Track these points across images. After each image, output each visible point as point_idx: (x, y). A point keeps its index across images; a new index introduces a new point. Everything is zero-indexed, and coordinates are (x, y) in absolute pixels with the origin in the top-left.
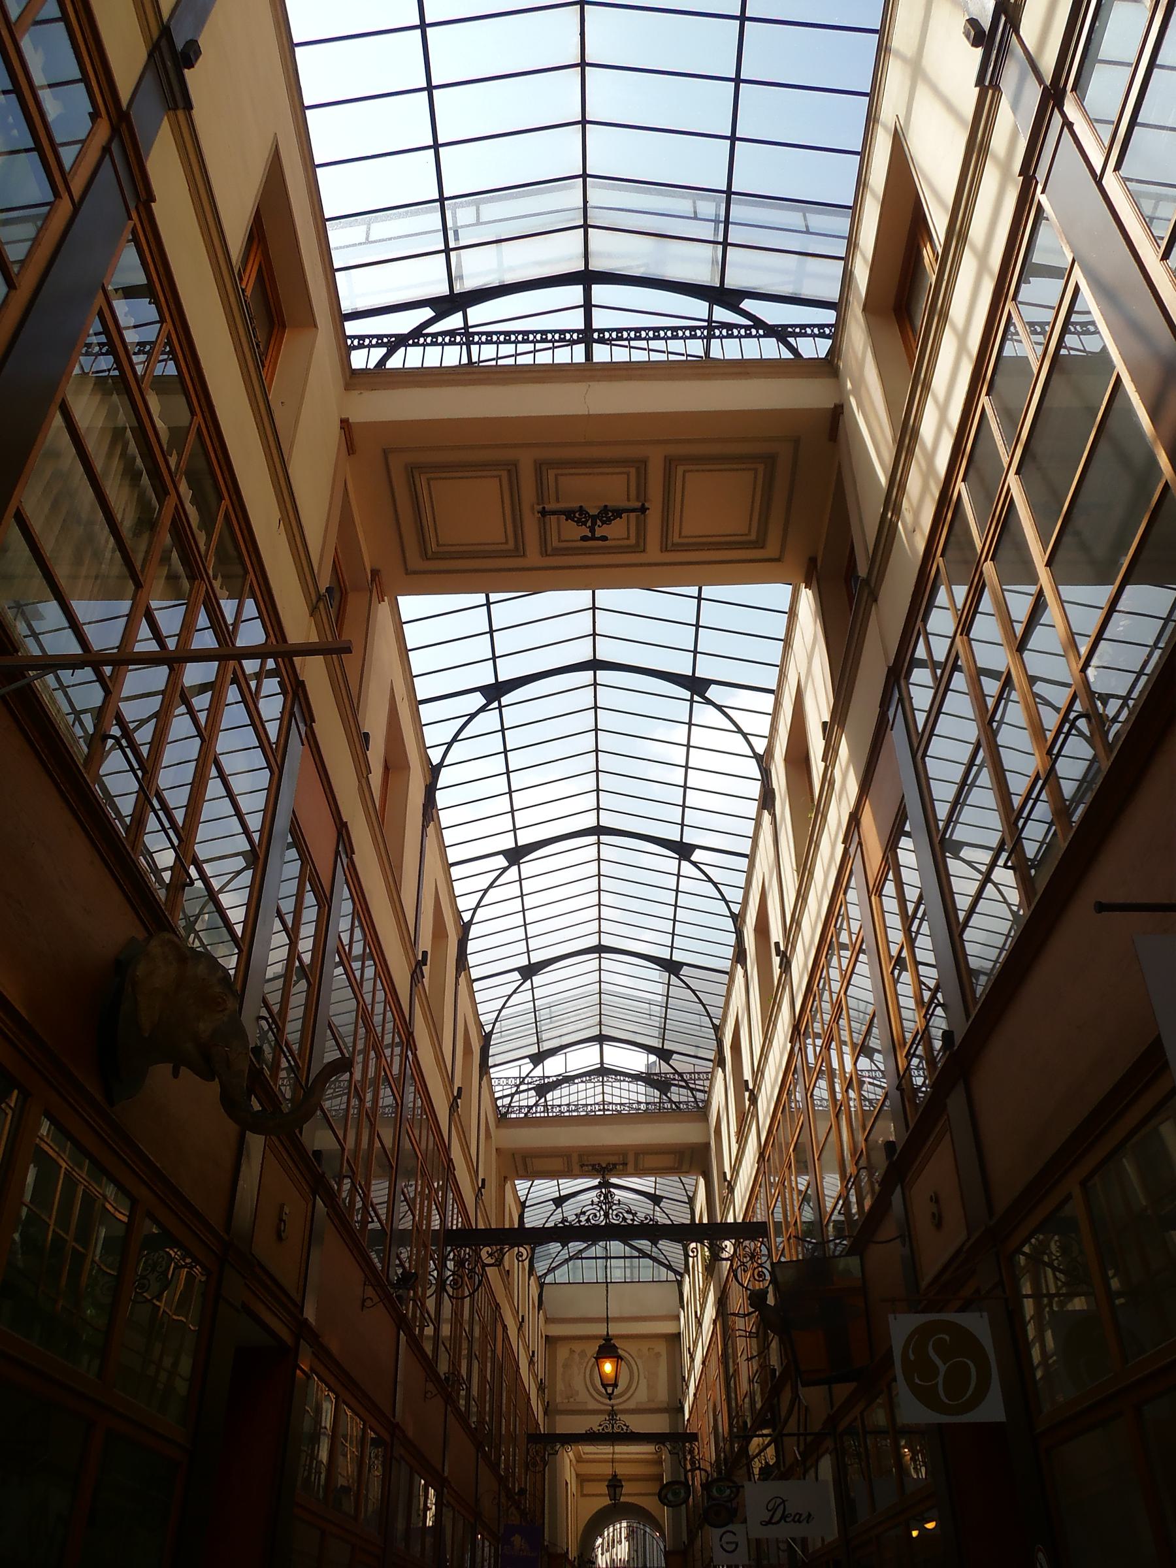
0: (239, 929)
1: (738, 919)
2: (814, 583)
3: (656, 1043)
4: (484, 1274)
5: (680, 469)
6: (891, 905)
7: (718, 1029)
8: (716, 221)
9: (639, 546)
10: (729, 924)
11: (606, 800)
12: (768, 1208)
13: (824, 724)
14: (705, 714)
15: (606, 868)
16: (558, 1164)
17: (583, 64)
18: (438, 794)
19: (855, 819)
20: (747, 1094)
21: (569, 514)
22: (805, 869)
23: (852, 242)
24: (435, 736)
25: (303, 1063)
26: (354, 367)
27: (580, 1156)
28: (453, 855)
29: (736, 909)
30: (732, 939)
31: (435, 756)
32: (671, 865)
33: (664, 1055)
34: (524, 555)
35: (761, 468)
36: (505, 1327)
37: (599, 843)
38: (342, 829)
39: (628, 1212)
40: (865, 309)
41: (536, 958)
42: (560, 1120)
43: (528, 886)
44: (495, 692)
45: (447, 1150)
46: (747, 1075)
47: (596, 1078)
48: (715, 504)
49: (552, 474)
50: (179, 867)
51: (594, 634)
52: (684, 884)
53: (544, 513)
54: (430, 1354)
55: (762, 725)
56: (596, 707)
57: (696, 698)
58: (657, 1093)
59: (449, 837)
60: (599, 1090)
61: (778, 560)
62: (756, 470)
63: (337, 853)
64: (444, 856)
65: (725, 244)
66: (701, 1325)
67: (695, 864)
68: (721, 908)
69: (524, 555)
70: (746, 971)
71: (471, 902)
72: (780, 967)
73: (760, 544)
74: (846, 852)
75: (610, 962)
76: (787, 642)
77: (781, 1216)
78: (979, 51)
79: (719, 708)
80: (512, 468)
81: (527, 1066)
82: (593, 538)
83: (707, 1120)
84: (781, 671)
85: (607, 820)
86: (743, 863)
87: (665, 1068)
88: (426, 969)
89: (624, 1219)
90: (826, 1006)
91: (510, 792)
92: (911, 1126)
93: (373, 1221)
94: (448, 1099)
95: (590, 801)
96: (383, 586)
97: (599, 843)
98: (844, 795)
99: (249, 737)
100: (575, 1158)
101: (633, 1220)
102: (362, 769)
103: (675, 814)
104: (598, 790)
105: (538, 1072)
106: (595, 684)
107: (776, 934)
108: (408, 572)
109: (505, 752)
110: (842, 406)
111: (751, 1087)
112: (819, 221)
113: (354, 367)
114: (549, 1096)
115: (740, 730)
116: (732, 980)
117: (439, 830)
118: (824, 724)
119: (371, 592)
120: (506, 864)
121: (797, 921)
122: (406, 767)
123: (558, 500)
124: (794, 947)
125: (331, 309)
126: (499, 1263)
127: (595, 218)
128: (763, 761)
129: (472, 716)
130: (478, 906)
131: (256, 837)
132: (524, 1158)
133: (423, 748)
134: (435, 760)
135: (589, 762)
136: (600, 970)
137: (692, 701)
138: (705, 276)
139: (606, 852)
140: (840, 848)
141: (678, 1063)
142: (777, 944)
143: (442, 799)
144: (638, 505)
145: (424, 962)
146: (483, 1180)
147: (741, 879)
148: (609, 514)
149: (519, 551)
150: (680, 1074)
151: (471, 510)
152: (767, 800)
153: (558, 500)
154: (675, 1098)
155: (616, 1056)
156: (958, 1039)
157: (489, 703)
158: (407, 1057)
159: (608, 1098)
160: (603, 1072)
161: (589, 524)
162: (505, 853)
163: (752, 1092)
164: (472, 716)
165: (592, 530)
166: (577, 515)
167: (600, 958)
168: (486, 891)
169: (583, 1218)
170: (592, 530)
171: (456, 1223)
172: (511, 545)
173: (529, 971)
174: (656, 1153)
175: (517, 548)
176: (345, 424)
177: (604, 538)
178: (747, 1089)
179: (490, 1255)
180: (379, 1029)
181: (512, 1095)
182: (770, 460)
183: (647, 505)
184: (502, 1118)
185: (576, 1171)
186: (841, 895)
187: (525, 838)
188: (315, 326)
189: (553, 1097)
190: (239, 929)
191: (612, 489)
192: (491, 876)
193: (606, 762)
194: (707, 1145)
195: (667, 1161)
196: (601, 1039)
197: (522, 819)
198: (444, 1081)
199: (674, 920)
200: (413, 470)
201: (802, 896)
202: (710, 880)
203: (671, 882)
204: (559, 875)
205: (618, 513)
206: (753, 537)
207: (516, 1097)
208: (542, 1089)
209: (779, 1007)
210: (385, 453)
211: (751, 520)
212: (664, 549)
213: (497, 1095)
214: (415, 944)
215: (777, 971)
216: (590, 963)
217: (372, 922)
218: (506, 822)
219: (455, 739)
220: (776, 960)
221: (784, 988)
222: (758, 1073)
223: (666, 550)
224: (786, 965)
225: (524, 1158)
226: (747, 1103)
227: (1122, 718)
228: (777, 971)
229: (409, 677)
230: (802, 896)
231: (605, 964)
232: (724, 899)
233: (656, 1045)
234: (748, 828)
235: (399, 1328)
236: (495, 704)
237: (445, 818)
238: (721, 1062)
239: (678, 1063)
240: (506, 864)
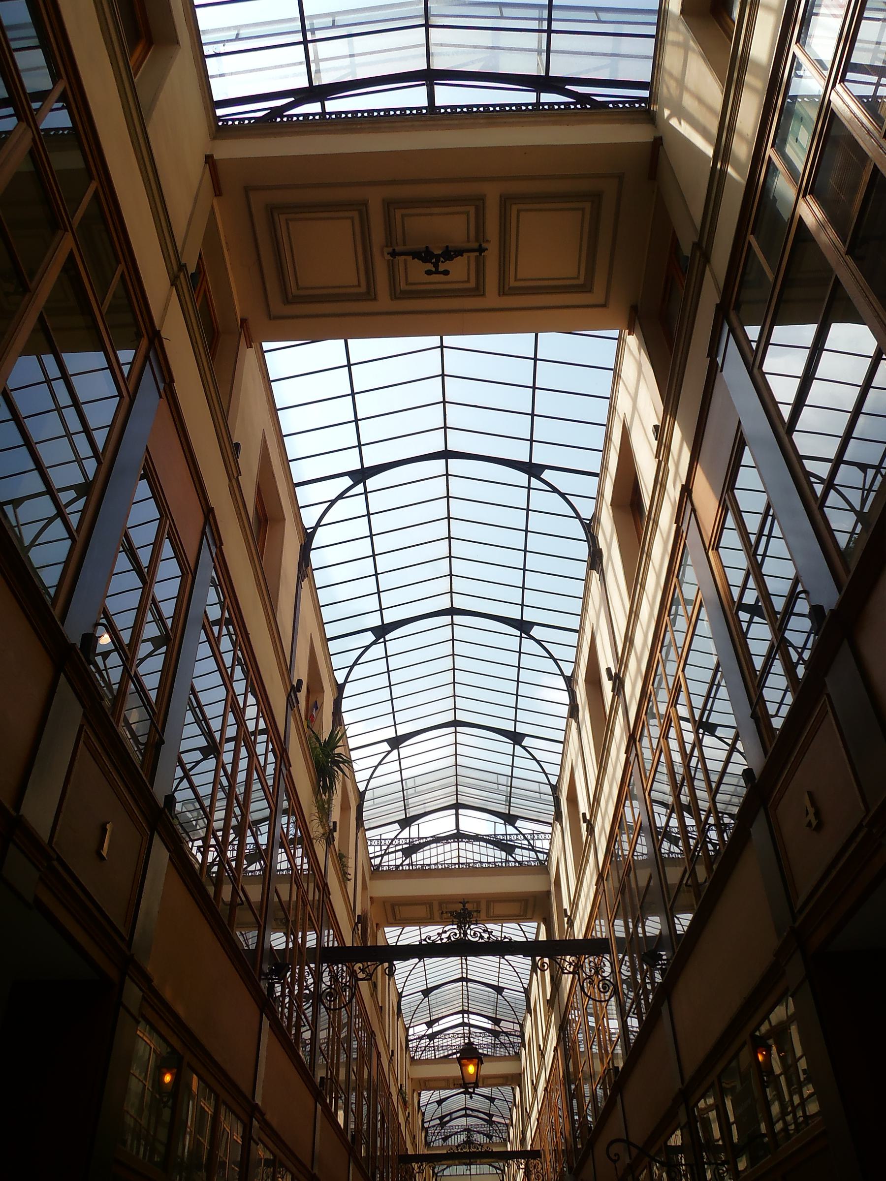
0: (153, 695)
1: (555, 789)
2: (638, 328)
3: (503, 809)
4: (357, 987)
5: (515, 208)
6: (674, 745)
7: (555, 789)
8: (539, 53)
9: (478, 291)
10: (548, 789)
11: (460, 703)
12: (583, 1005)
13: (656, 427)
14: (529, 645)
15: (460, 663)
16: (422, 911)
17: (443, 375)
18: (365, 804)
19: (687, 490)
20: (566, 919)
21: (416, 255)
22: (542, 1065)
23: (604, 466)
24: (309, 518)
25: (160, 711)
26: (215, 100)
27: (440, 904)
28: (331, 631)
29: (554, 780)
30: (565, 697)
31: (340, 677)
32: (508, 747)
33: (496, 1021)
34: (375, 299)
35: (588, 206)
36: (379, 1054)
37: (456, 732)
38: (209, 513)
39: (485, 931)
40: (612, 504)
41: (412, 812)
42: (425, 872)
43: (394, 663)
44: (381, 631)
45: (389, 1087)
46: (566, 905)
47: (453, 840)
48: (546, 245)
49: (398, 213)
50: (123, 683)
51: (450, 538)
52: (526, 661)
53: (394, 254)
54: (212, 896)
55: (571, 654)
56: (451, 575)
57: (523, 635)
58: (504, 854)
59: (324, 596)
60: (455, 853)
61: (604, 306)
62: (583, 210)
63: (204, 533)
64: (319, 616)
65: (549, 31)
66: (536, 1091)
67: (524, 748)
68: (542, 778)
69: (375, 299)
70: (562, 827)
71: (367, 774)
72: (613, 691)
73: (586, 288)
74: (627, 759)
75: (465, 736)
76: (585, 599)
77: (623, 929)
78: (611, 682)
79: (538, 642)
80: (362, 207)
81: (424, 1027)
82: (437, 272)
83: (520, 1060)
84: (585, 585)
85: (460, 602)
86: (559, 747)
87: (511, 830)
88: (336, 835)
89: (481, 937)
90: (673, 655)
91: (395, 725)
92: (770, 750)
93: (305, 1026)
94: (351, 925)
95: (450, 703)
96: (251, 335)
97: (456, 732)
98: (665, 536)
99: (211, 664)
100: (451, 1081)
101: (489, 938)
102: (233, 474)
103: (511, 713)
104: (456, 743)
105: (405, 834)
106: (452, 624)
107: (583, 807)
108: (271, 317)
109: (390, 686)
110: (661, 138)
111: (569, 914)
112: (627, 45)
113: (215, 100)
114: (414, 856)
115: (552, 657)
116: (587, 589)
117: (314, 589)
118: (656, 427)
119: (240, 334)
120: (390, 749)
121: (629, 639)
122: (322, 690)
123: (404, 244)
124: (596, 818)
125: (204, 97)
126: (369, 977)
127: (433, 21)
128: (570, 681)
129: (367, 648)
130: (371, 777)
131: (169, 622)
132: (393, 906)
133: (355, 783)
134: (362, 789)
135: (449, 690)
136: (457, 775)
137: (521, 637)
138: (531, 66)
139: (459, 633)
140: (623, 756)
141: (526, 827)
142: (584, 814)
143: (316, 559)
144: (475, 245)
145: (298, 688)
146: (392, 1051)
147: (558, 759)
148: (450, 254)
149: (370, 295)
150: (524, 835)
151: (327, 252)
152: (595, 560)
153: (404, 244)
154: (519, 858)
155: (475, 1020)
156: (757, 772)
157: (378, 639)
158: (281, 770)
159: (462, 860)
160: (458, 836)
161: (434, 260)
162: (373, 630)
163: (569, 918)
164: (367, 648)
165: (436, 265)
166: (425, 255)
167: (457, 815)
168: (376, 767)
169: (444, 936)
170: (436, 265)
171: (329, 940)
172: (363, 289)
173: (396, 742)
174: (505, 901)
175: (368, 293)
176: (209, 159)
177: (446, 273)
178: (566, 915)
179: (362, 970)
180: (262, 759)
181: (382, 856)
182: (596, 198)
183: (484, 245)
184: (376, 872)
185: (452, 1086)
186: (675, 579)
187: (390, 617)
188: (178, 43)
189: (418, 858)
190: (153, 695)
191: (453, 227)
192: (379, 758)
193: (459, 567)
194: (549, 892)
195: (514, 908)
196: (462, 1012)
197: (388, 599)
198: (280, 668)
199: (513, 755)
200: (272, 210)
201: (633, 615)
202: (534, 759)
203: (513, 659)
204: (427, 757)
205: (460, 252)
206: (581, 281)
207: (386, 858)
208: (412, 849)
209: (587, 860)
210: (247, 190)
211: (582, 226)
212: (503, 291)
213: (371, 856)
214: (290, 670)
215: (584, 834)
216: (446, 737)
217: (294, 784)
218: (372, 603)
219: (355, 663)
220: (584, 826)
221: (590, 846)
222: (574, 904)
223: (504, 294)
224: (591, 830)
225: (393, 906)
226: (566, 926)
227: (809, 645)
228: (608, 694)
229: (322, 624)
230: (633, 615)
231: (461, 738)
232: (544, 772)
233: (503, 811)
234: (578, 588)
235: (349, 1155)
236: (382, 640)
237: (320, 578)
238: (558, 816)
239: (502, 1024)
240: (390, 749)
